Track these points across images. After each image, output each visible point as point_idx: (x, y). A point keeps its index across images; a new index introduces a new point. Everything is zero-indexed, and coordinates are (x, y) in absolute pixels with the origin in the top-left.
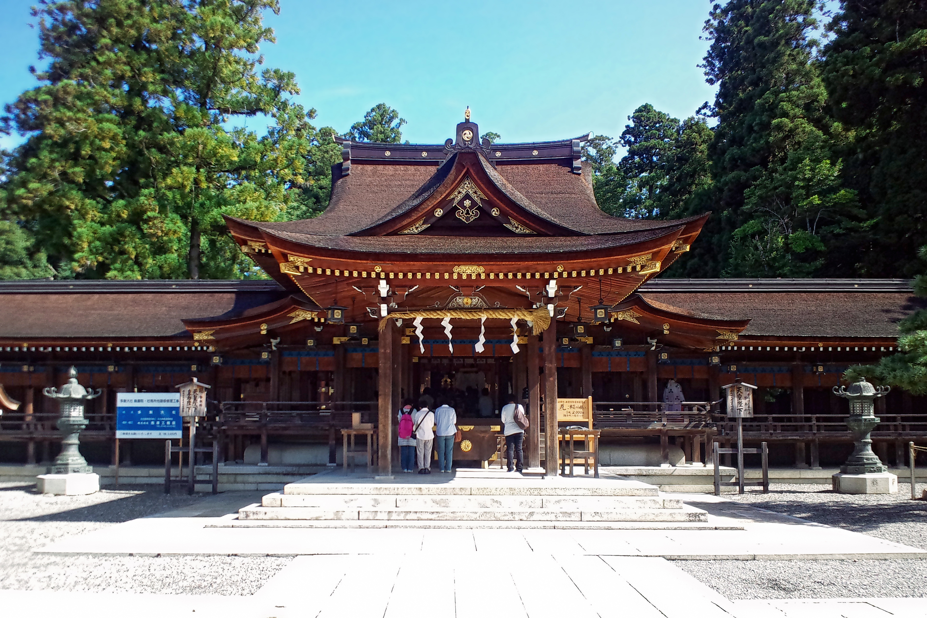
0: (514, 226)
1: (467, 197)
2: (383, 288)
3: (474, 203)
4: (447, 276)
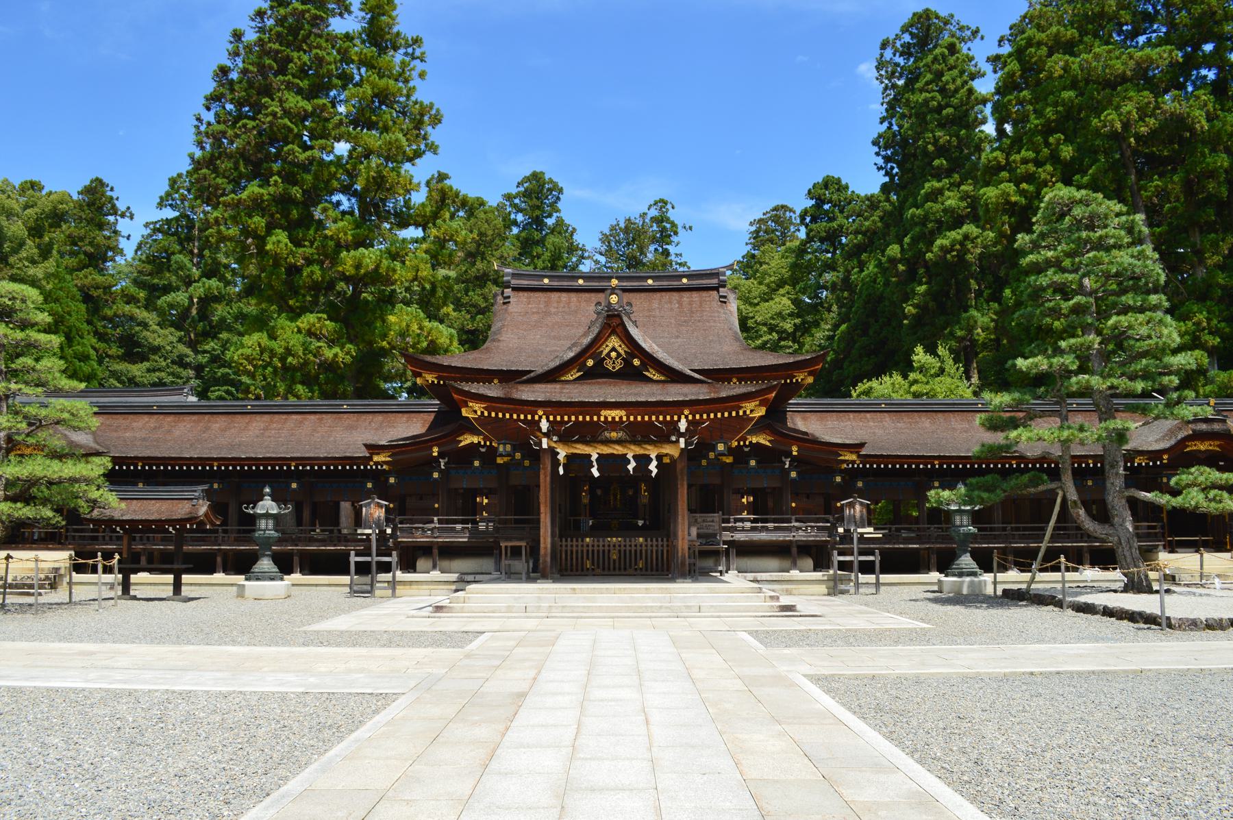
0: (652, 374)
1: (614, 349)
2: (544, 425)
3: (619, 355)
4: (595, 418)
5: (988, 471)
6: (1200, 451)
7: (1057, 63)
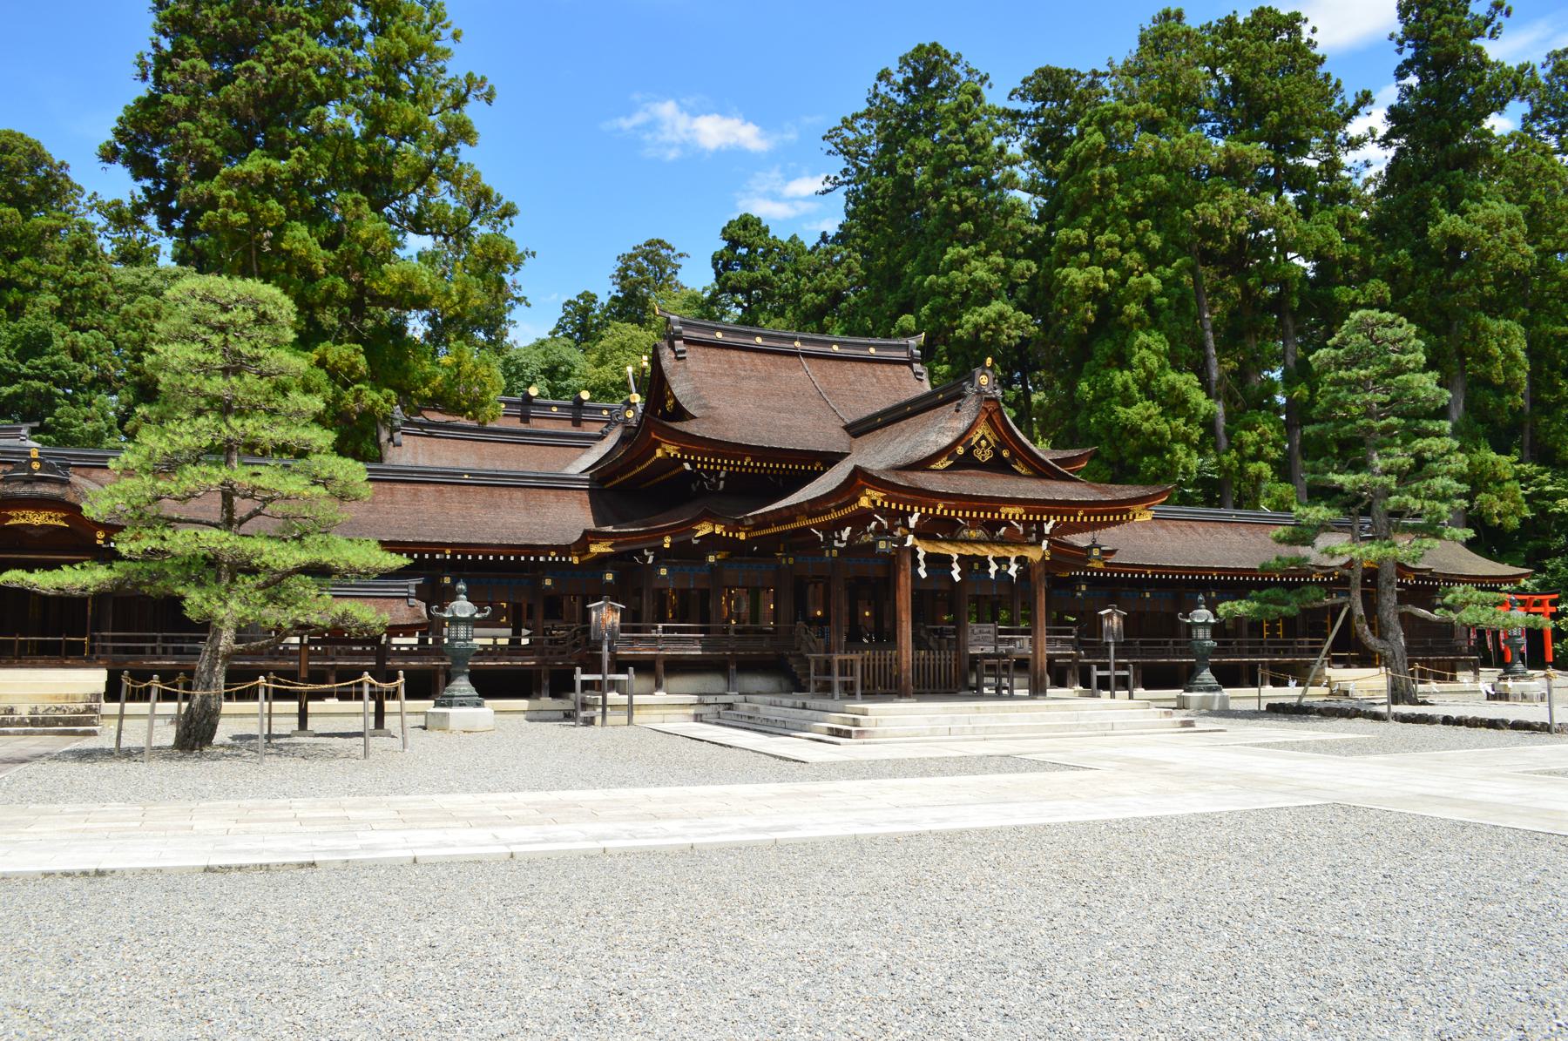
1: (983, 437)
5: (1269, 585)
6: (31, 526)
7: (1146, 143)
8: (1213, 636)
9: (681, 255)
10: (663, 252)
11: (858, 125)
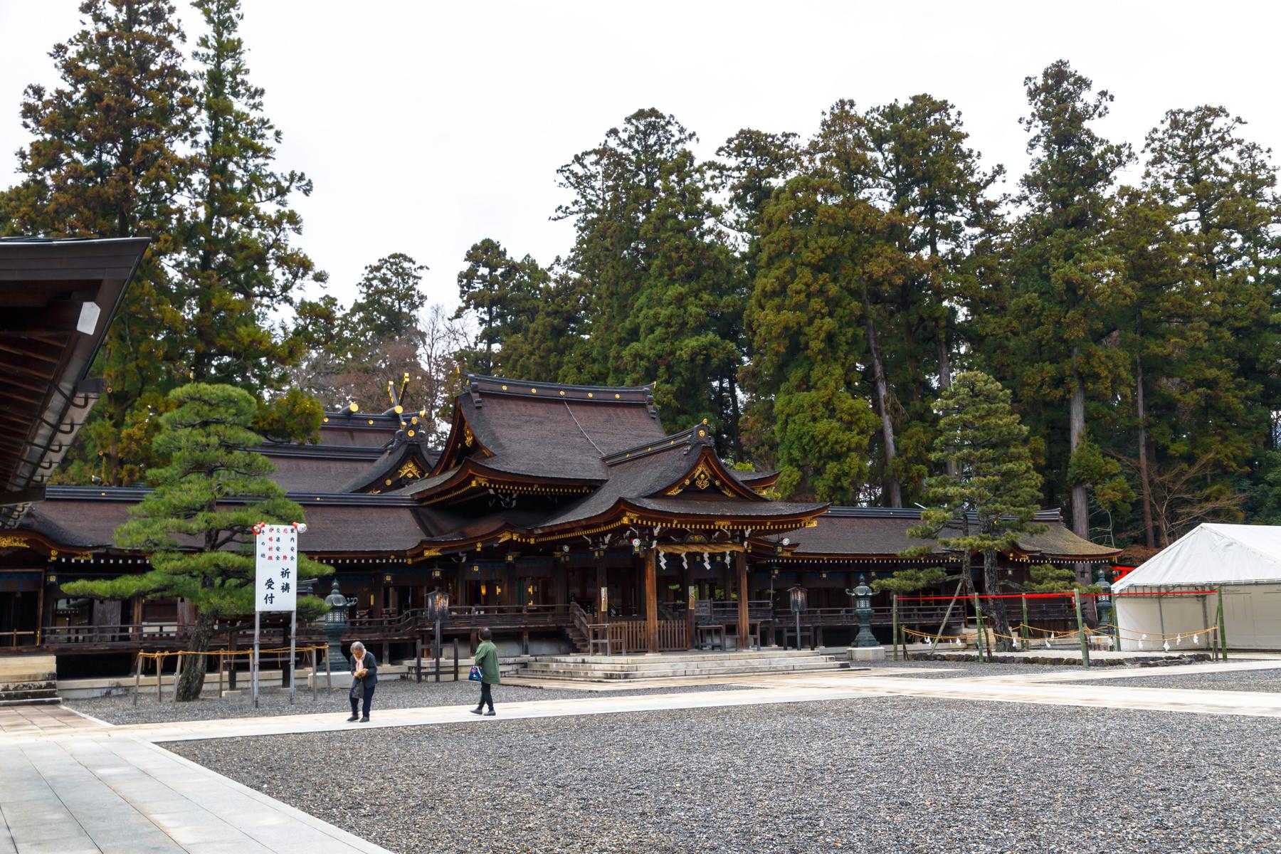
8: (872, 605)
9: (421, 268)
10: (406, 265)
11: (586, 162)
